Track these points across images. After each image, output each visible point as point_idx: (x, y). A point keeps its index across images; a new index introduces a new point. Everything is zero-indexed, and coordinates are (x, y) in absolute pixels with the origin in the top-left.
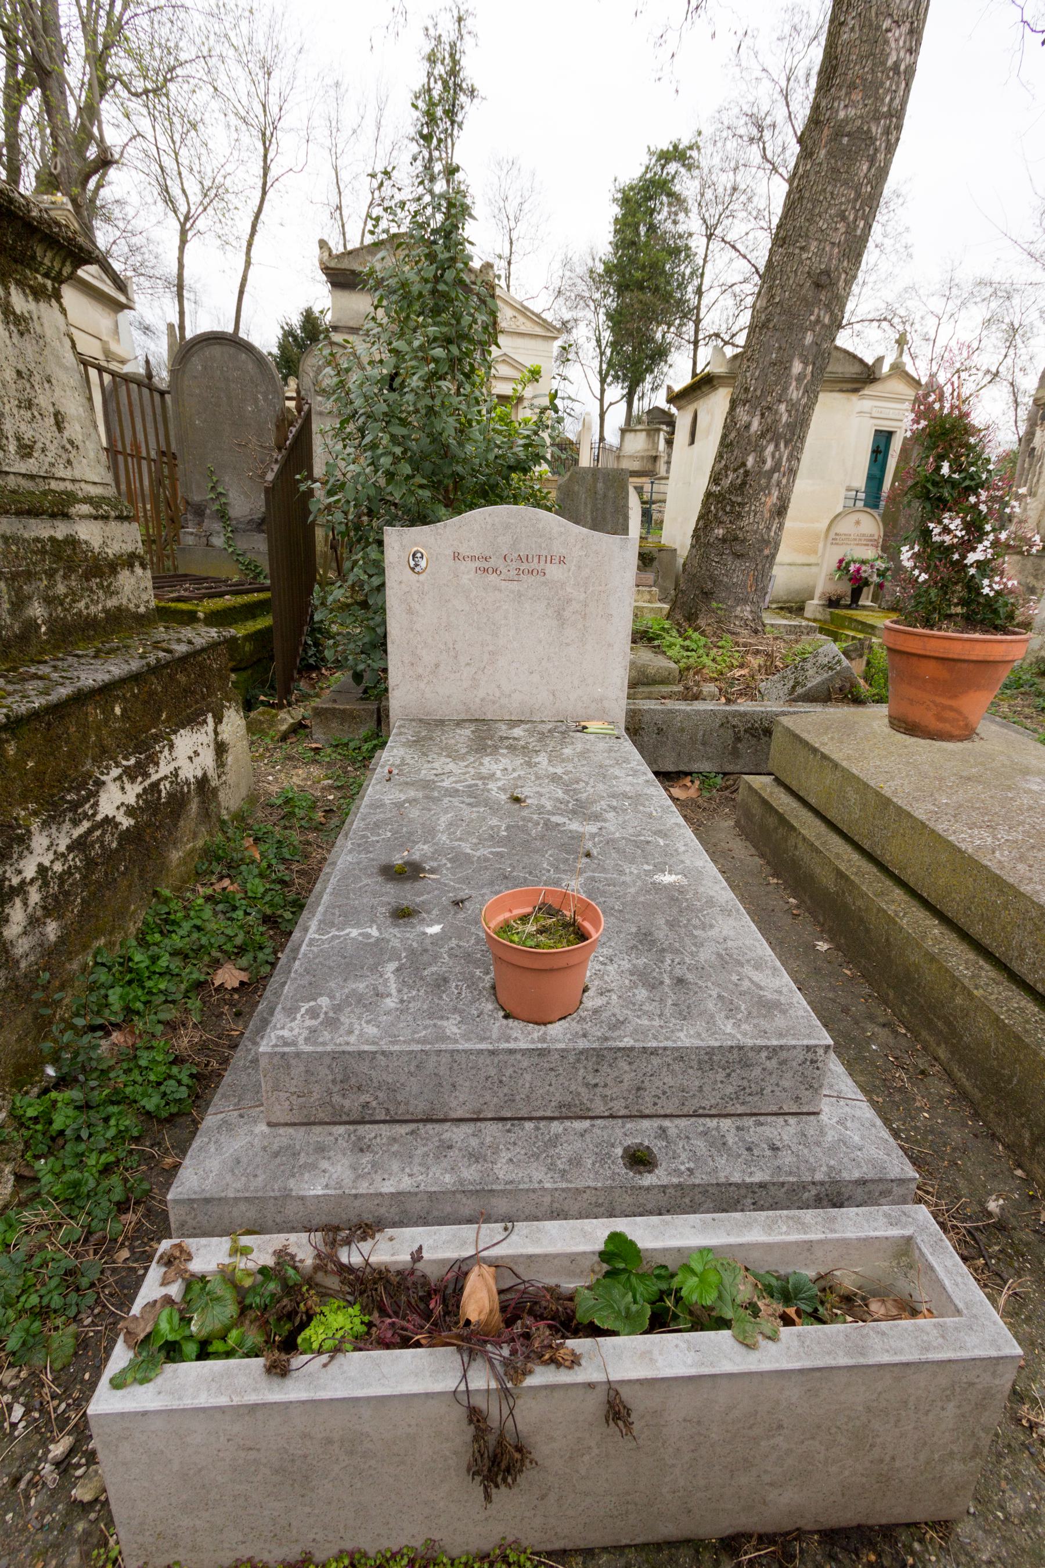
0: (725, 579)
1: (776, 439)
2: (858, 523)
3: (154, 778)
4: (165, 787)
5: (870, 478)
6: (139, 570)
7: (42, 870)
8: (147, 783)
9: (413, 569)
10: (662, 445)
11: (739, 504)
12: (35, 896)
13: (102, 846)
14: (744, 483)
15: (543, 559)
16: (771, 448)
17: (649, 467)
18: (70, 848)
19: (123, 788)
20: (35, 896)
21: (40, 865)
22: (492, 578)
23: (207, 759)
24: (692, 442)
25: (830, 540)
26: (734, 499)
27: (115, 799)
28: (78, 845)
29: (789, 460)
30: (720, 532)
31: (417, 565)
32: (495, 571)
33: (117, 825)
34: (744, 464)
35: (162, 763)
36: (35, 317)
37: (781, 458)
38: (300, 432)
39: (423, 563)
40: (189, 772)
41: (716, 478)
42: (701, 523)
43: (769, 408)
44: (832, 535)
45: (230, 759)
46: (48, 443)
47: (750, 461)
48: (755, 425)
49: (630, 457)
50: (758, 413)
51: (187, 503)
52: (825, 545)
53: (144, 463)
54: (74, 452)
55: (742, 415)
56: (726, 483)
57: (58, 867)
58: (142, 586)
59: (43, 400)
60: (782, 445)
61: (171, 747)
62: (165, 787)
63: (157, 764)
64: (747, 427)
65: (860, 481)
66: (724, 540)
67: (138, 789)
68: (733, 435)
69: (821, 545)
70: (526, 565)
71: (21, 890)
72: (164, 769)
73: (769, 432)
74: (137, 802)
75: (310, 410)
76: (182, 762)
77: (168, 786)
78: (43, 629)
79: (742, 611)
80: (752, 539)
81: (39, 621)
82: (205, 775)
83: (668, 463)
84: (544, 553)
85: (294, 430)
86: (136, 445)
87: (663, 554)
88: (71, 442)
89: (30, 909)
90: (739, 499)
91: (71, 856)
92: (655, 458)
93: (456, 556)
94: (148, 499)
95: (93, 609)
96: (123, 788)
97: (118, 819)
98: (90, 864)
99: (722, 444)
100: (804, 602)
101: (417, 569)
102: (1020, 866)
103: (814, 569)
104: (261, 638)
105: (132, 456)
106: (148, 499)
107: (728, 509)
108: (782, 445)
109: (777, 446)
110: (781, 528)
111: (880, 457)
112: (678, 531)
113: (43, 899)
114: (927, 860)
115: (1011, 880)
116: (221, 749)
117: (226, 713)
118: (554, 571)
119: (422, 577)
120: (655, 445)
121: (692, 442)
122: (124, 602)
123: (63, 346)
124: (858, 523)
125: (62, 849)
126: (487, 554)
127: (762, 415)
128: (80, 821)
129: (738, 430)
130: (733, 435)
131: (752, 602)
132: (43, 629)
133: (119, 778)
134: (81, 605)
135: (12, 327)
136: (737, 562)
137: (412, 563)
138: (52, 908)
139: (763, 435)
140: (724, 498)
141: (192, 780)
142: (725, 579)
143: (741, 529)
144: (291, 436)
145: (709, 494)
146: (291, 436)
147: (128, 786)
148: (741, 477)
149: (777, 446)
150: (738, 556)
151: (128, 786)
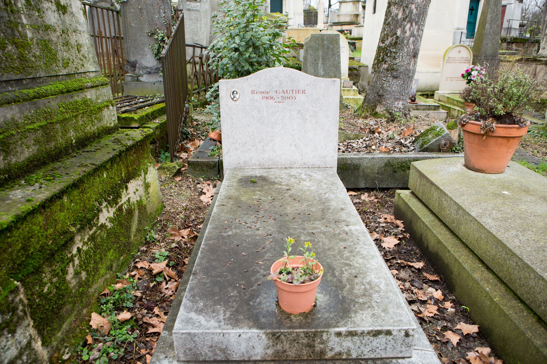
0: (389, 89)
1: (411, 21)
2: (459, 52)
3: (120, 204)
4: (125, 207)
5: (469, 23)
6: (111, 107)
7: (79, 250)
8: (118, 206)
9: (233, 99)
10: (361, 8)
11: (394, 52)
12: (77, 262)
13: (101, 238)
14: (396, 43)
15: (294, 92)
16: (408, 26)
17: (354, 19)
18: (89, 239)
19: (108, 211)
20: (77, 262)
21: (78, 248)
22: (271, 102)
23: (141, 190)
24: (374, 12)
25: (446, 61)
26: (392, 50)
27: (106, 216)
28: (92, 238)
29: (418, 31)
30: (385, 66)
31: (234, 97)
32: (272, 98)
33: (106, 226)
34: (396, 34)
35: (123, 196)
36: (69, 5)
37: (413, 30)
38: (178, 28)
39: (237, 96)
40: (134, 199)
41: (382, 40)
42: (376, 61)
43: (407, 7)
44: (446, 58)
45: (151, 190)
46: (74, 58)
47: (399, 33)
48: (400, 16)
49: (344, 15)
50: (401, 9)
51: (128, 62)
52: (443, 63)
53: (104, 40)
54: (85, 60)
55: (394, 10)
56: (387, 42)
57: (85, 248)
58: (112, 114)
59: (73, 41)
60: (414, 24)
61: (127, 188)
62: (125, 207)
63: (121, 198)
64: (397, 15)
65: (463, 24)
66: (387, 70)
67: (114, 210)
68: (390, 19)
69: (442, 63)
70: (288, 95)
71: (72, 260)
72: (124, 199)
73: (408, 18)
74: (114, 216)
75: (183, 16)
76: (131, 195)
77: (126, 207)
78: (74, 141)
79: (398, 104)
80: (402, 69)
81: (72, 138)
82: (141, 199)
83: (364, 17)
84: (295, 89)
85: (175, 27)
86: (100, 32)
87: (361, 68)
88: (83, 56)
89: (75, 267)
90: (394, 50)
91: (89, 243)
92: (357, 16)
93: (253, 92)
94: (105, 55)
95: (93, 129)
96: (108, 211)
97: (107, 224)
98: (97, 247)
99: (384, 23)
100: (434, 91)
101: (235, 99)
102: (516, 240)
103: (439, 75)
104: (162, 126)
105: (98, 37)
106: (105, 55)
107: (389, 55)
108: (414, 24)
109: (411, 26)
110: (415, 63)
111: (474, 12)
112: (368, 55)
113: (79, 263)
114: (477, 236)
115: (511, 248)
116: (147, 186)
117: (149, 169)
118: (301, 97)
119: (237, 103)
120: (357, 9)
121: (374, 12)
122: (105, 123)
123: (80, 14)
124: (459, 52)
125: (86, 240)
126: (268, 91)
127: (404, 10)
128: (92, 227)
129: (392, 17)
130: (390, 19)
131: (403, 100)
132: (74, 141)
133: (107, 206)
134: (88, 128)
135: (60, 12)
136: (395, 81)
137: (232, 96)
138: (84, 265)
139: (404, 20)
140: (387, 49)
141: (136, 202)
142: (389, 89)
143: (396, 64)
144: (173, 31)
145: (379, 48)
146: (173, 31)
147: (110, 209)
148: (395, 39)
149: (411, 26)
150: (395, 77)
151: (110, 209)
